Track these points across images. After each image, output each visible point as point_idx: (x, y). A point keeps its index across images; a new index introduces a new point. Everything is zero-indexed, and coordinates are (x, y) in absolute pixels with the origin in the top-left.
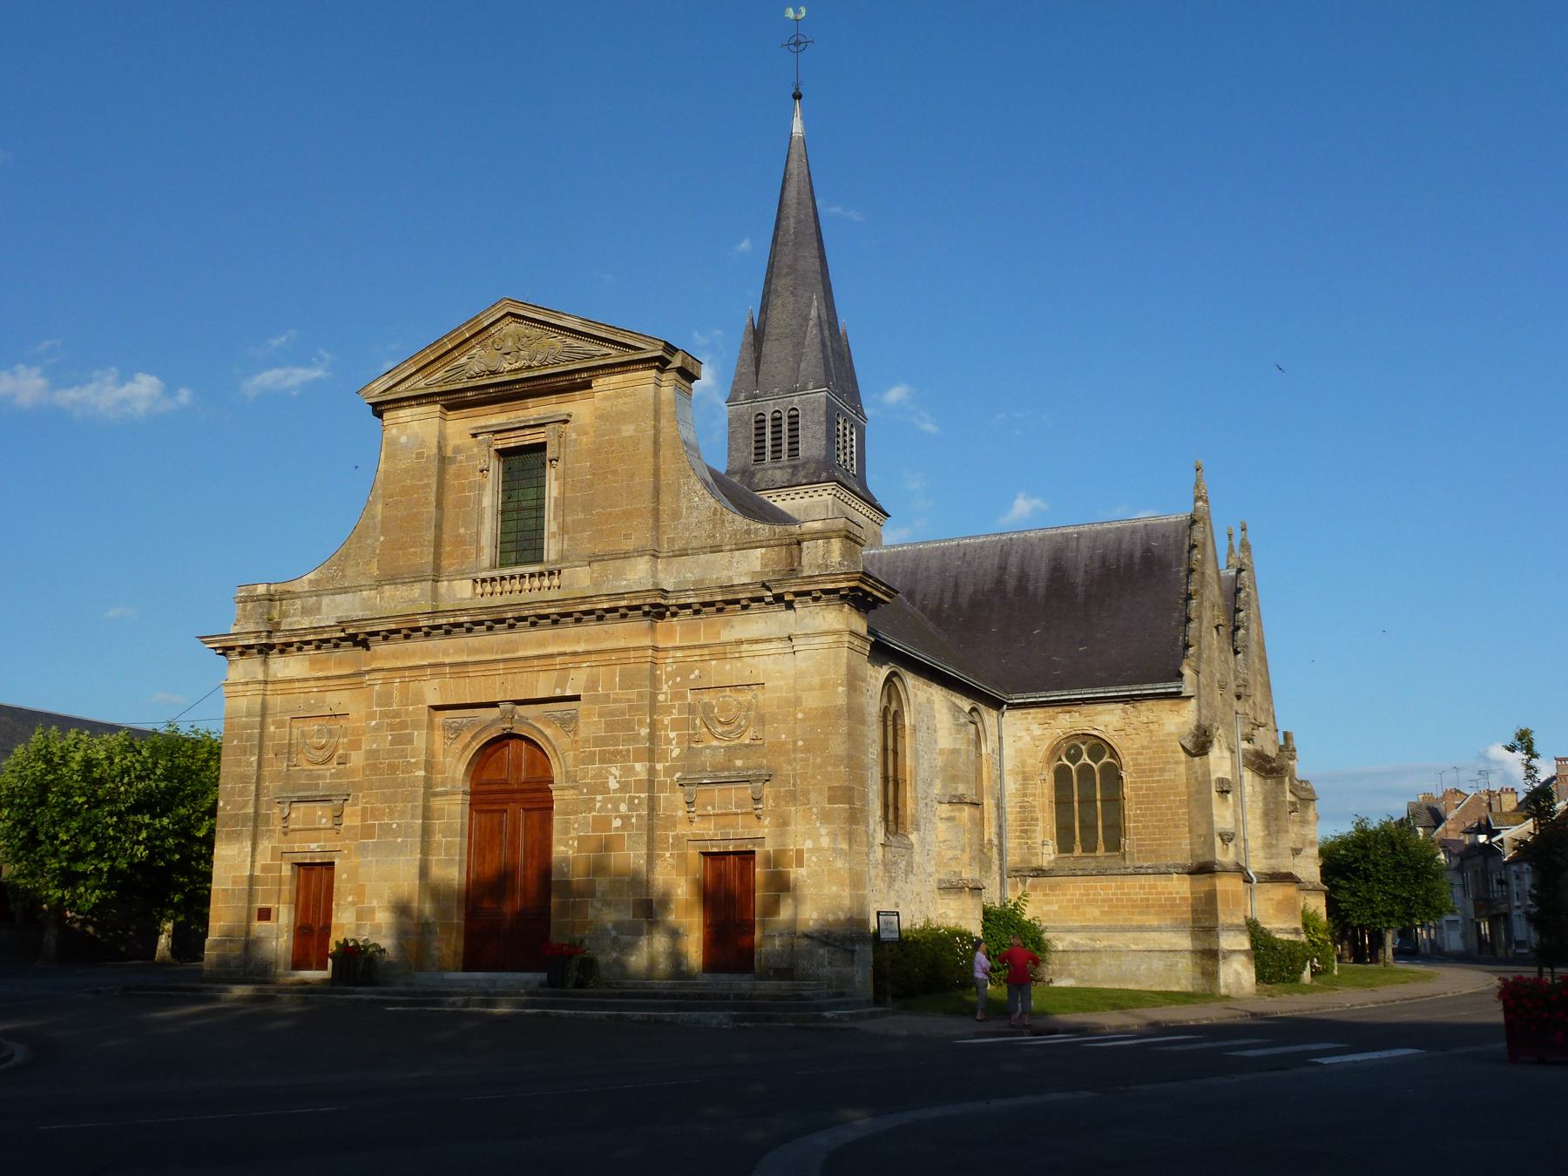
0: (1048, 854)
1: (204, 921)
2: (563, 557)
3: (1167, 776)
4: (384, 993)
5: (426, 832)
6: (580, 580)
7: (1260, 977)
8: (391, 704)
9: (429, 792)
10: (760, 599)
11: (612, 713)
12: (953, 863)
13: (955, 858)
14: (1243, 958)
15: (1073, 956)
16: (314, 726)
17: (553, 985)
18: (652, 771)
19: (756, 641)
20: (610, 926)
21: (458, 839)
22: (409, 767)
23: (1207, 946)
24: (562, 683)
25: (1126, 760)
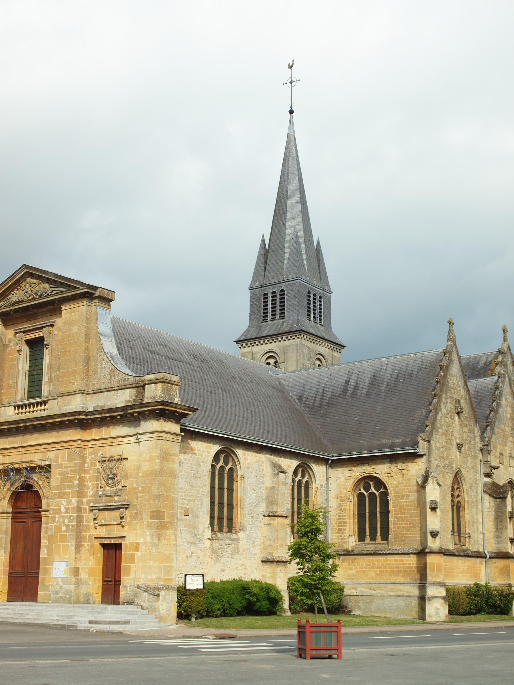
2: (50, 394)
7: (451, 612)
11: (63, 473)
12: (270, 548)
13: (270, 545)
14: (441, 601)
18: (80, 502)
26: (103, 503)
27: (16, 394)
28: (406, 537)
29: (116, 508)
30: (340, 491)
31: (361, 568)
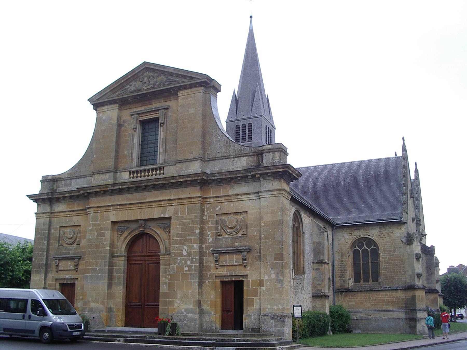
0: (351, 283)
1: (57, 300)
3: (396, 253)
4: (92, 335)
5: (111, 272)
6: (170, 171)
8: (96, 221)
9: (112, 256)
10: (246, 177)
11: (184, 224)
12: (318, 286)
13: (319, 284)
15: (360, 321)
16: (68, 230)
17: (160, 334)
18: (201, 248)
19: (244, 194)
20: (183, 310)
21: (123, 275)
22: (104, 246)
23: (412, 316)
24: (164, 212)
25: (381, 247)
26: (223, 248)
27: (132, 162)
28: (394, 279)
29: (240, 252)
30: (341, 248)
31: (360, 301)
